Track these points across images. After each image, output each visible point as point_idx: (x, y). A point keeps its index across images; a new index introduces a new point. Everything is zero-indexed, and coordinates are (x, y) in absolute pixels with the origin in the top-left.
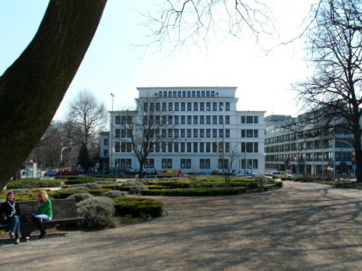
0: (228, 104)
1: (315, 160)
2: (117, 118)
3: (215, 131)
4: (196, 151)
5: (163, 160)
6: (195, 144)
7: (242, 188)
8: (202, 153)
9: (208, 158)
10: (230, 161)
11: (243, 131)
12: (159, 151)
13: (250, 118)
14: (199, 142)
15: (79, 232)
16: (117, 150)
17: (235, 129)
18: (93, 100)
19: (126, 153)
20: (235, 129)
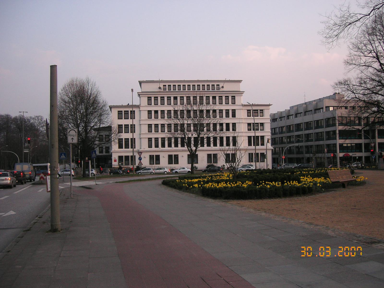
0: (234, 98)
1: (315, 141)
2: (335, 145)
3: (163, 112)
4: (163, 146)
5: (150, 156)
6: (228, 138)
7: (357, 99)
8: (157, 149)
9: (215, 153)
10: (265, 153)
11: (249, 124)
12: (216, 146)
13: (255, 111)
14: (218, 136)
15: (218, 200)
16: (120, 147)
17: (242, 119)
18: (89, 89)
19: (124, 149)
20: (242, 119)
